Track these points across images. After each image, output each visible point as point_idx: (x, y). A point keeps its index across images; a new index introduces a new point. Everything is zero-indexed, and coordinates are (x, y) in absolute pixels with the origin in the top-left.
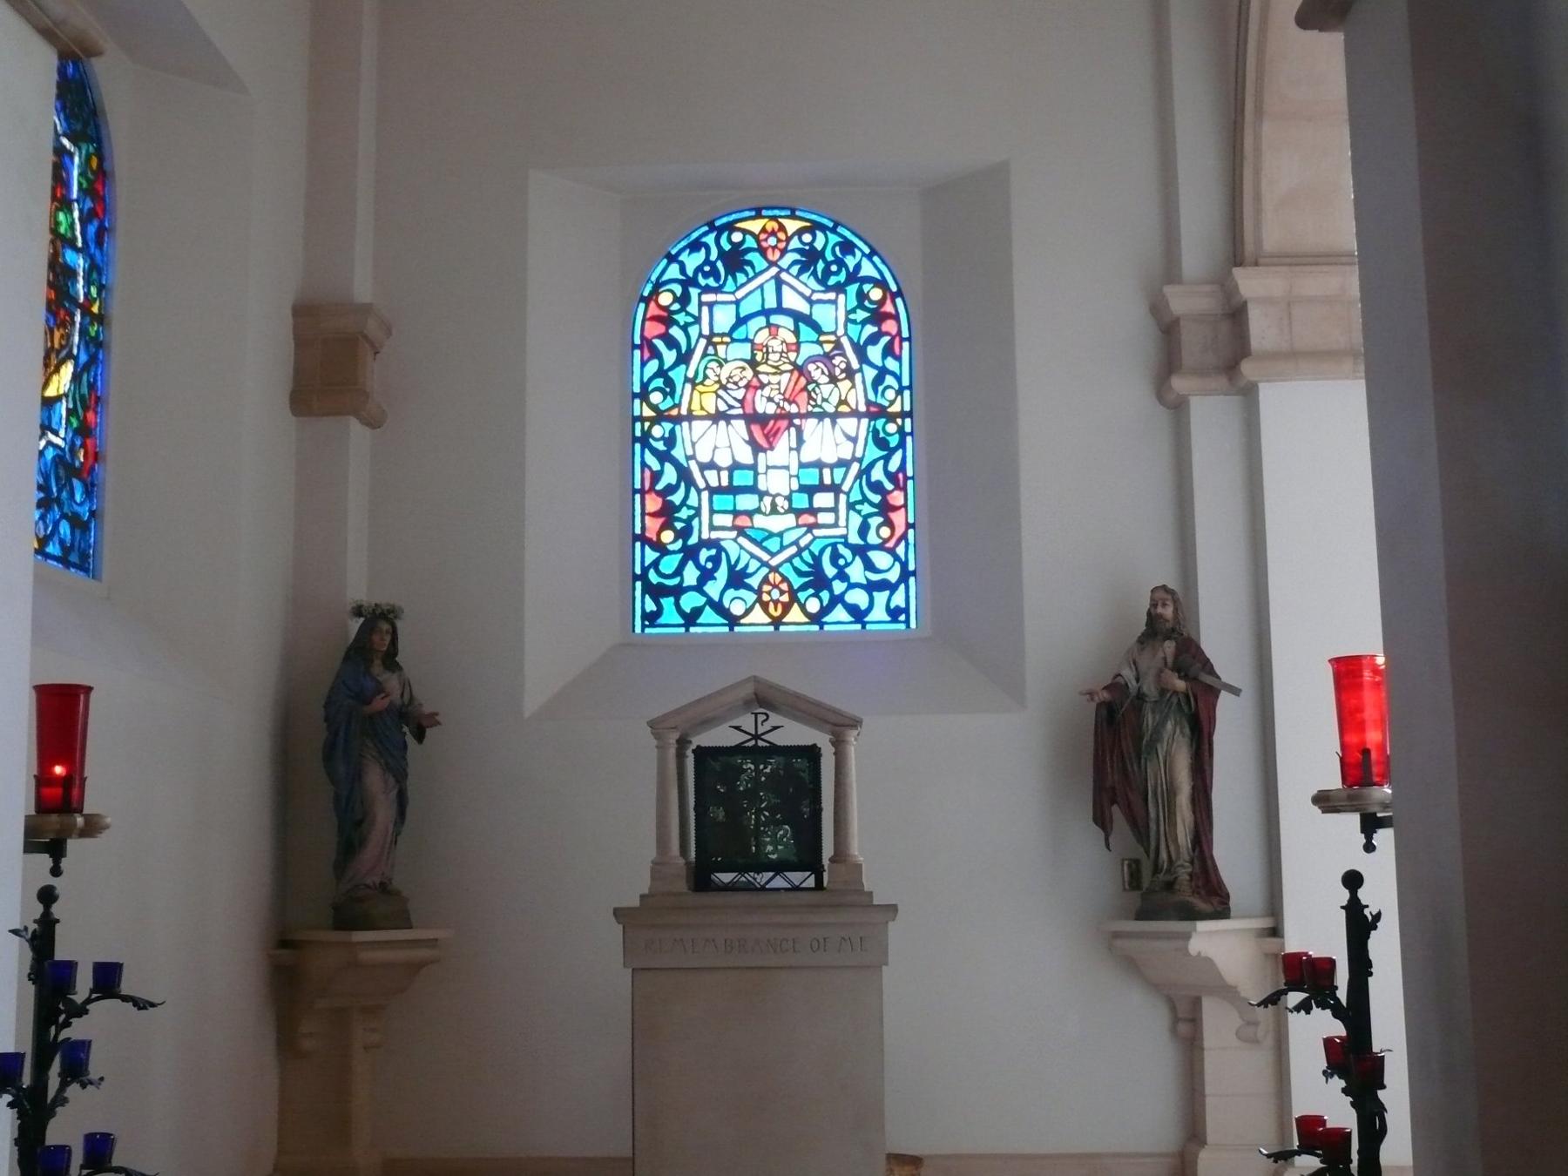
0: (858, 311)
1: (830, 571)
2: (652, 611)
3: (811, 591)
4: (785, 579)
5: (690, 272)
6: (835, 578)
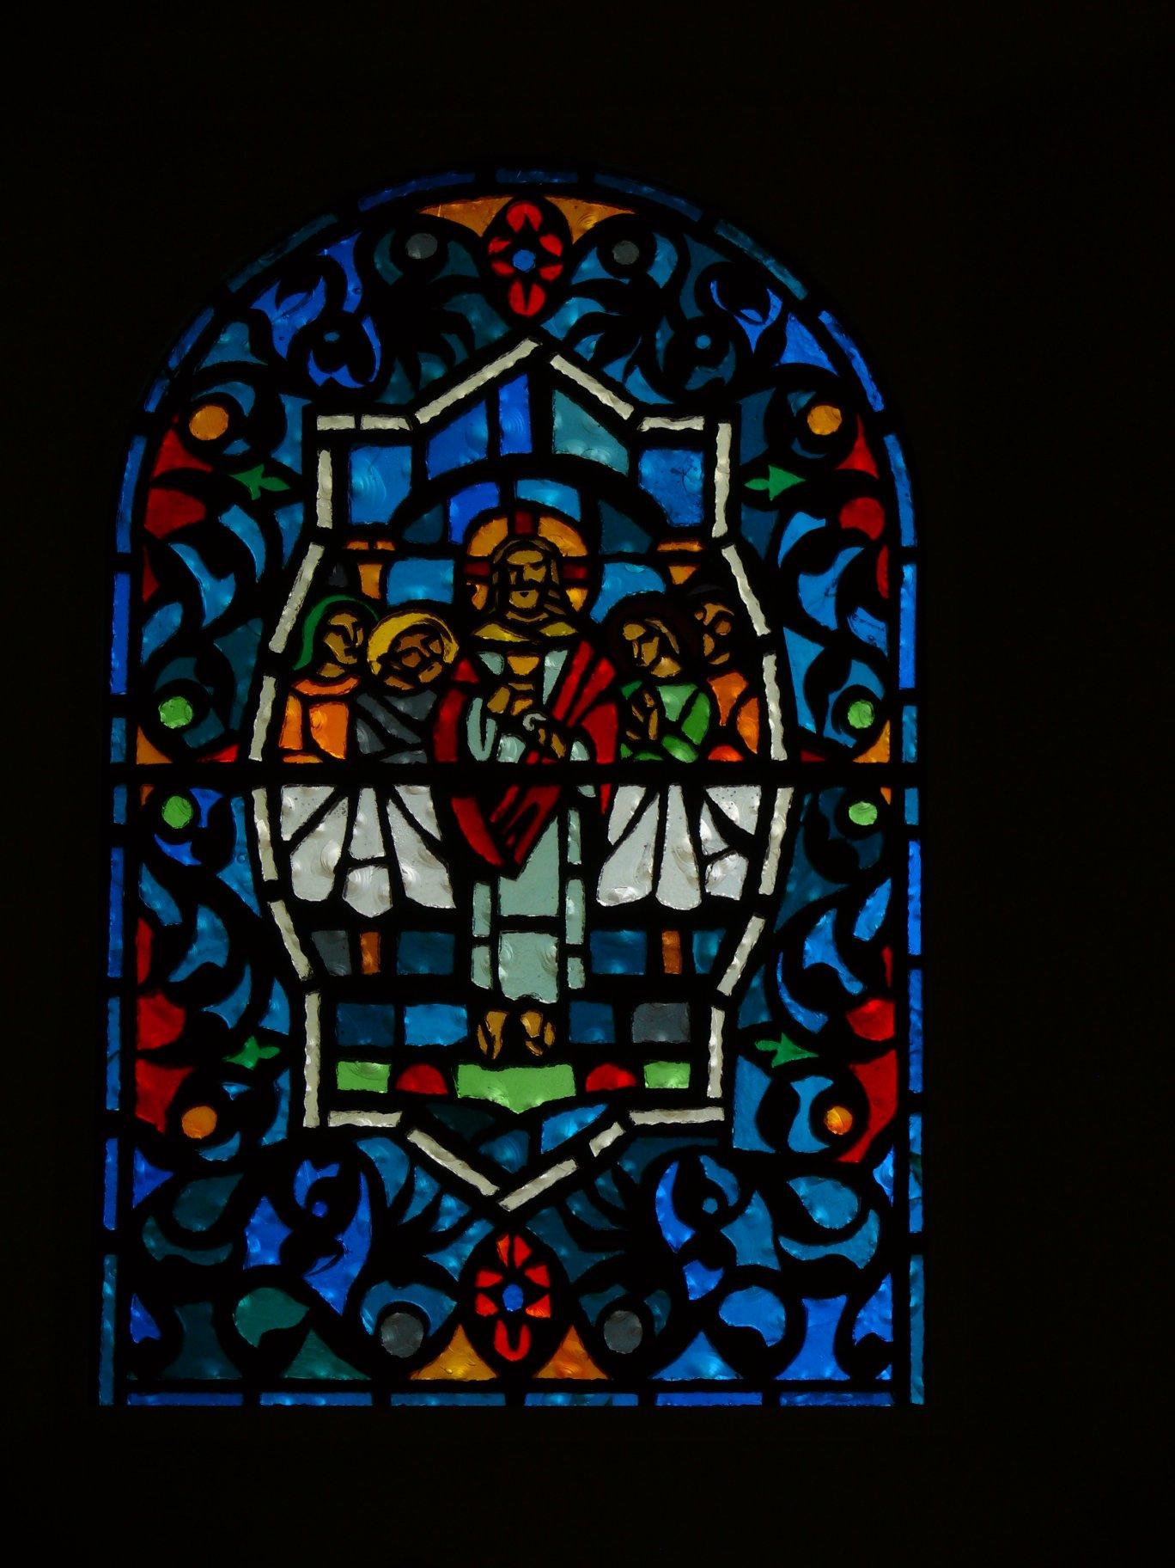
2: (147, 1340)
3: (617, 1292)
4: (542, 1254)
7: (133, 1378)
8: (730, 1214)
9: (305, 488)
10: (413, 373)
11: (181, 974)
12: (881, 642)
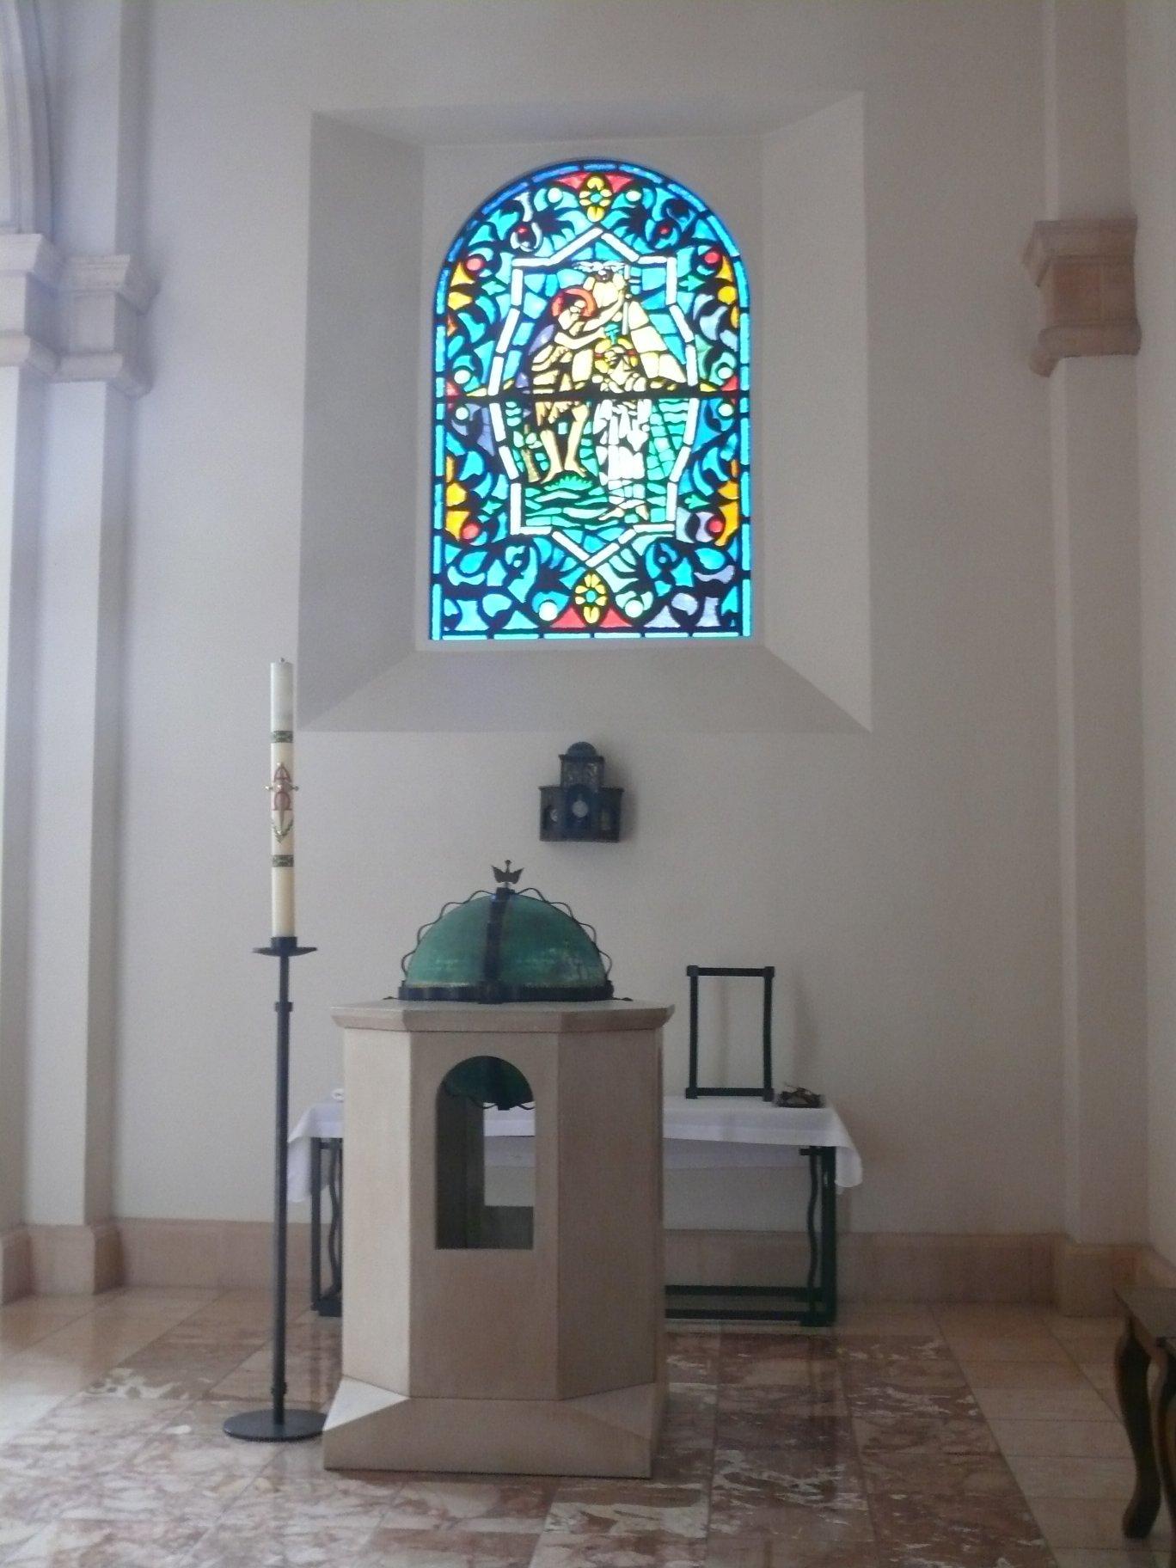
1: (653, 571)
8: (674, 565)
9: (508, 289)
12: (734, 347)
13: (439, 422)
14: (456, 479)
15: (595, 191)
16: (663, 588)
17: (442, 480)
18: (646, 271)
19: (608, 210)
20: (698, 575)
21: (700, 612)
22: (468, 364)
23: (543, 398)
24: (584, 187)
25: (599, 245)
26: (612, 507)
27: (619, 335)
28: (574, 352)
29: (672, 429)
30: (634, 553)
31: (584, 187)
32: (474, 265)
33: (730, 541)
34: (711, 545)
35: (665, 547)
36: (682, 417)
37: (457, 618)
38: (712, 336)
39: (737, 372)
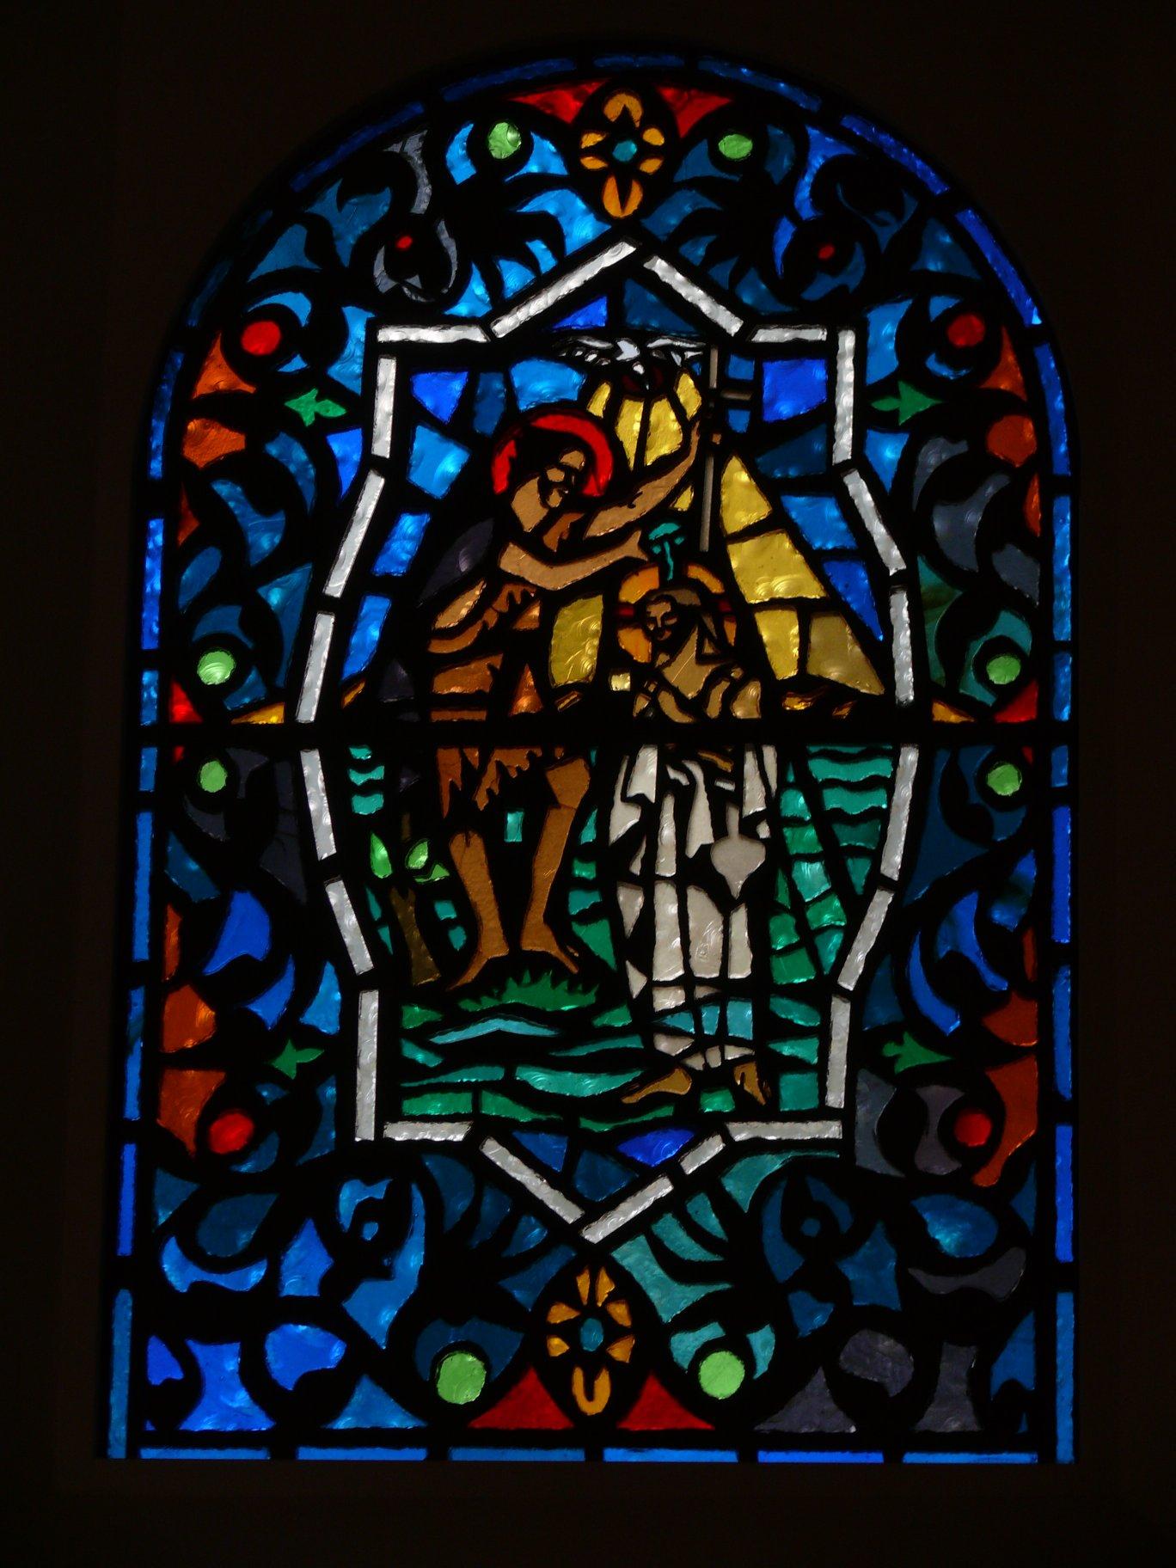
0: (903, 387)
1: (783, 1261)
2: (169, 1382)
3: (712, 1331)
4: (628, 1288)
5: (345, 247)
6: (796, 1283)
7: (149, 1427)
8: (850, 1244)
9: (360, 412)
10: (494, 283)
11: (215, 966)
12: (1032, 591)
13: (146, 801)
14: (191, 973)
15: (624, 128)
16: (813, 1317)
17: (151, 975)
18: (772, 370)
19: (658, 190)
20: (919, 1274)
21: (922, 1389)
22: (233, 628)
23: (459, 735)
24: (592, 117)
25: (632, 289)
26: (666, 1065)
27: (688, 553)
28: (554, 602)
29: (847, 837)
30: (724, 1205)
31: (592, 117)
32: (261, 339)
33: (1015, 1171)
34: (958, 1186)
35: (819, 1190)
36: (877, 799)
37: (190, 1390)
38: (967, 560)
39: (1037, 668)
